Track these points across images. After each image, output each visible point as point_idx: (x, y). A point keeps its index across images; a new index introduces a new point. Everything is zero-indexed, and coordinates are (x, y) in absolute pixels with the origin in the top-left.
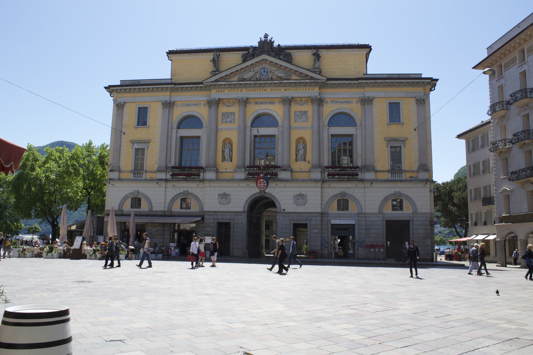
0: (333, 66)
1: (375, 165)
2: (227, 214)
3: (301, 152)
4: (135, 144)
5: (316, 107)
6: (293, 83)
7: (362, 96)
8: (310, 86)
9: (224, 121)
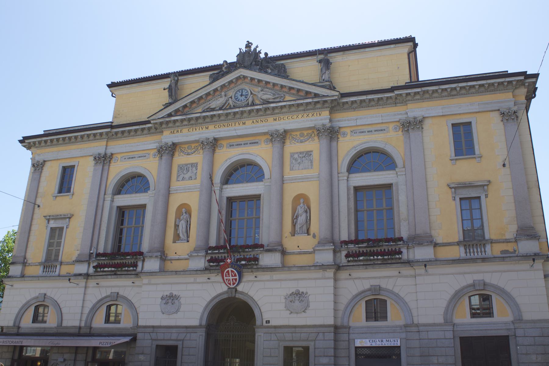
0: (352, 76)
1: (433, 233)
2: (174, 330)
3: (302, 219)
4: (52, 222)
5: (325, 141)
6: (285, 106)
7: (403, 117)
8: (314, 109)
9: (181, 178)
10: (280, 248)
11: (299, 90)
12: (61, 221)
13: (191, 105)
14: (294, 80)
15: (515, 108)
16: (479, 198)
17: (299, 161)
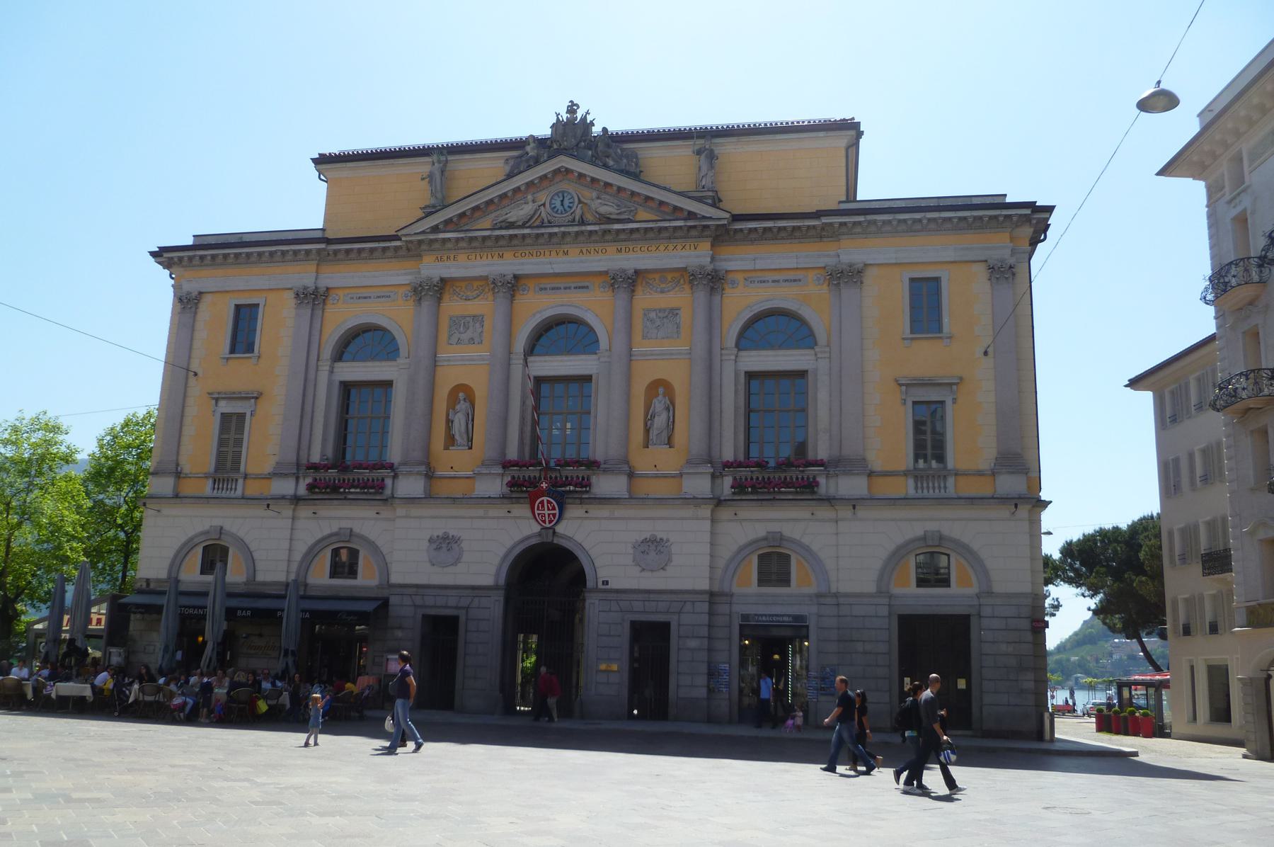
3: (660, 421)
4: (222, 403)
5: (701, 295)
6: (637, 229)
7: (831, 261)
9: (454, 339)
10: (626, 468)
11: (661, 203)
12: (240, 403)
13: (472, 214)
14: (654, 185)
15: (1012, 261)
16: (942, 403)
17: (658, 323)
